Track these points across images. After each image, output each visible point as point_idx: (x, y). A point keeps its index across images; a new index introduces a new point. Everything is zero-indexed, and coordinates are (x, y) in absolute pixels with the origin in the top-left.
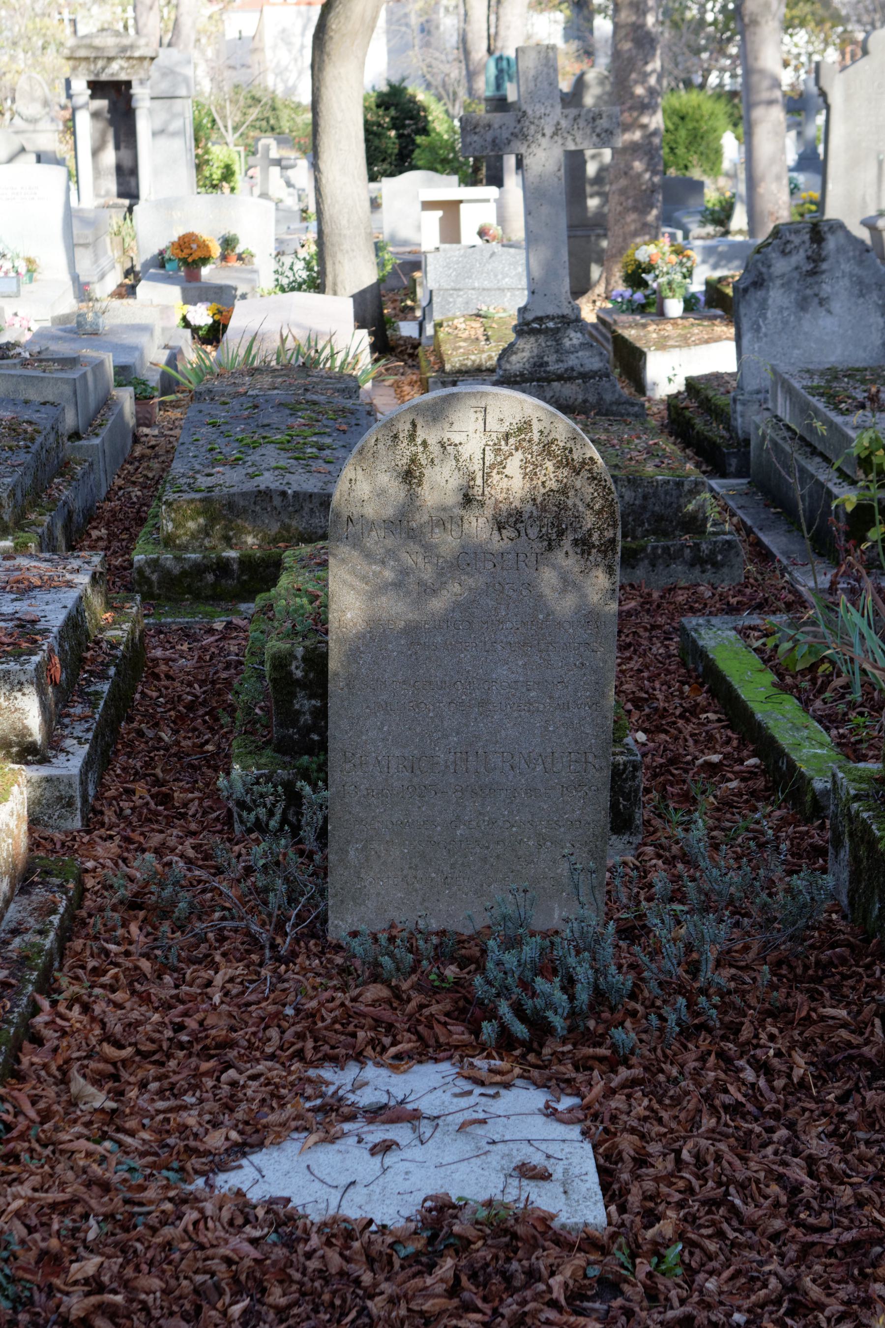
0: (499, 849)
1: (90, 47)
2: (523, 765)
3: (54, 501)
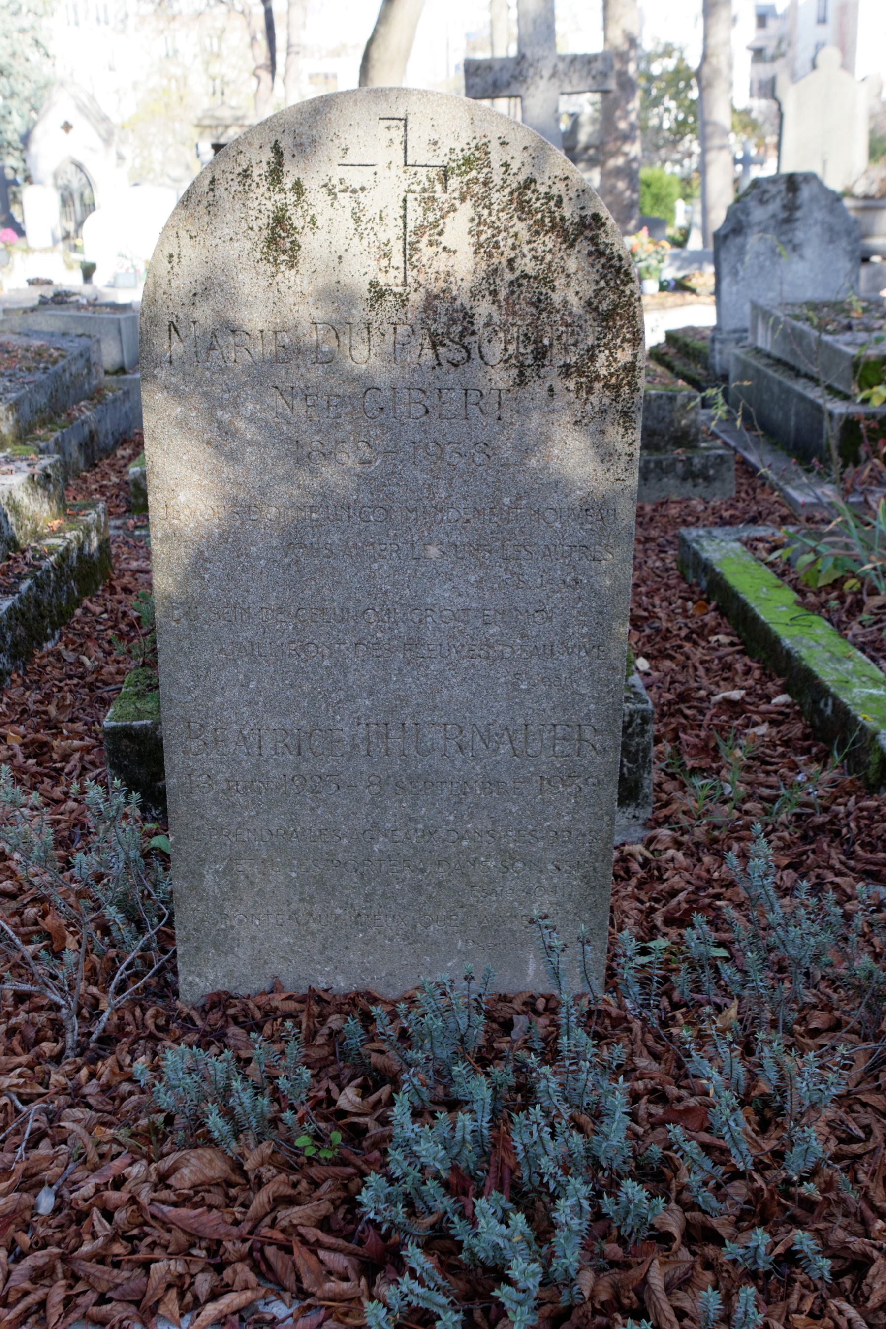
0: (442, 872)
1: (212, 117)
2: (479, 745)
3: (71, 419)
